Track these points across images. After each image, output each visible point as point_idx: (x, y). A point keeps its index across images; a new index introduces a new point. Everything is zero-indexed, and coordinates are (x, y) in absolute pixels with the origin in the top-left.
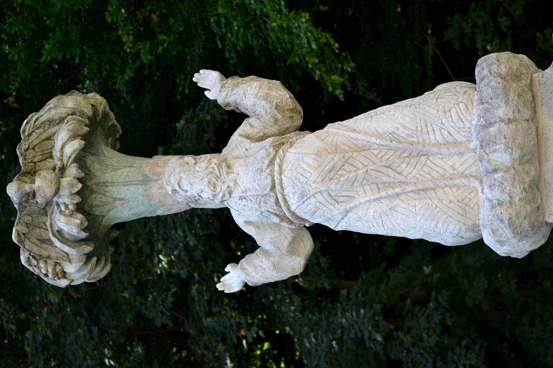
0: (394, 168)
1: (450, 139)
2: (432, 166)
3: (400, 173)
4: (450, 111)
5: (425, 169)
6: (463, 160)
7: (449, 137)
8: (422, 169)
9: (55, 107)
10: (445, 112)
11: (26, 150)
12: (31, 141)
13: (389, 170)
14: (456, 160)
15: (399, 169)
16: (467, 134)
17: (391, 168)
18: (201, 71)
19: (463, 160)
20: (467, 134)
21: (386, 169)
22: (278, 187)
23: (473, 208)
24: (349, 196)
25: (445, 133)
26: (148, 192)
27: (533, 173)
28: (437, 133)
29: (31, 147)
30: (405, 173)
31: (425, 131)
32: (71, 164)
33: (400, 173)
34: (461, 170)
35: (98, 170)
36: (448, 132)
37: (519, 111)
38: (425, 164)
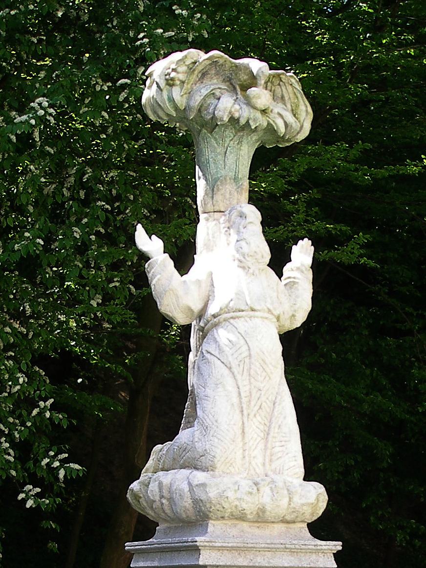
0: (259, 411)
1: (274, 458)
2: (258, 441)
3: (255, 416)
4: (296, 461)
5: (255, 436)
6: (260, 465)
7: (276, 458)
8: (256, 433)
9: (307, 111)
10: (295, 457)
11: (280, 78)
12: (287, 85)
13: (258, 407)
14: (260, 460)
15: (258, 415)
16: (278, 471)
17: (259, 409)
18: (313, 247)
19: (260, 465)
20: (278, 471)
21: (259, 405)
22: (252, 313)
23: (228, 468)
24: (243, 371)
25: (280, 455)
26: (229, 181)
27: (249, 517)
28: (281, 449)
29: (281, 83)
30: (254, 420)
31: (282, 439)
32: (268, 121)
33: (255, 416)
34: (253, 463)
35: (251, 138)
36: (280, 457)
37: (294, 512)
38: (258, 436)
